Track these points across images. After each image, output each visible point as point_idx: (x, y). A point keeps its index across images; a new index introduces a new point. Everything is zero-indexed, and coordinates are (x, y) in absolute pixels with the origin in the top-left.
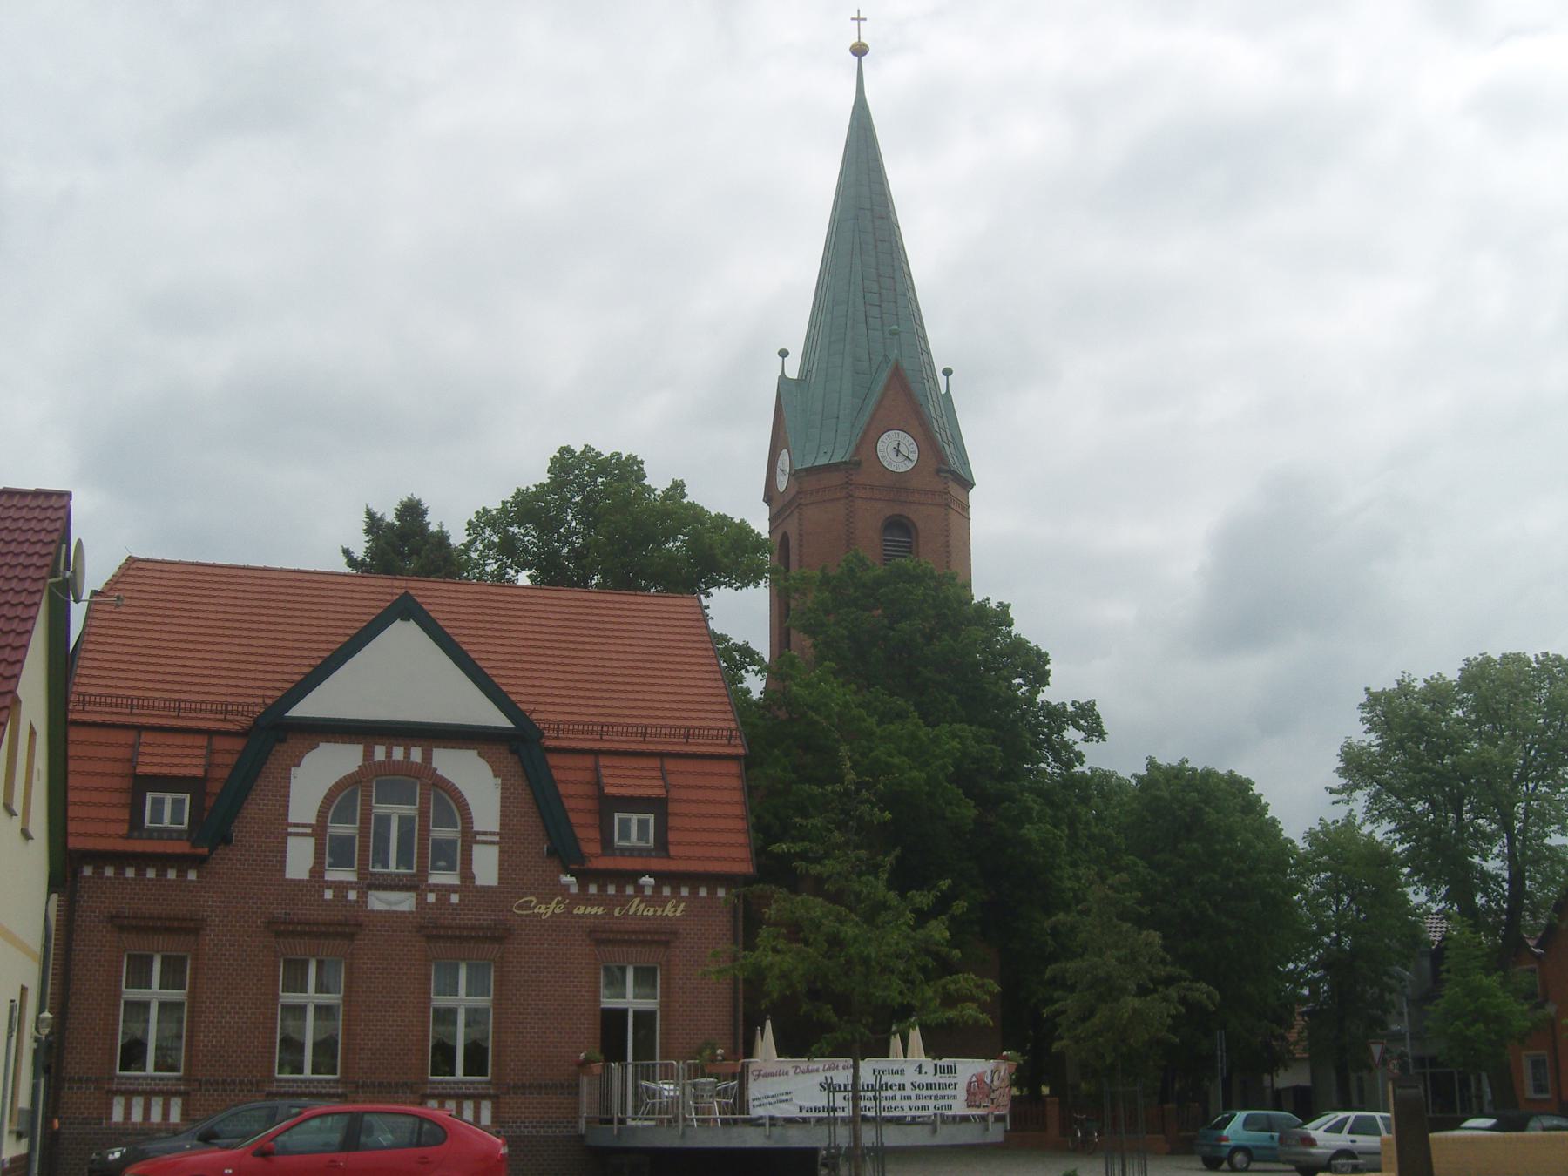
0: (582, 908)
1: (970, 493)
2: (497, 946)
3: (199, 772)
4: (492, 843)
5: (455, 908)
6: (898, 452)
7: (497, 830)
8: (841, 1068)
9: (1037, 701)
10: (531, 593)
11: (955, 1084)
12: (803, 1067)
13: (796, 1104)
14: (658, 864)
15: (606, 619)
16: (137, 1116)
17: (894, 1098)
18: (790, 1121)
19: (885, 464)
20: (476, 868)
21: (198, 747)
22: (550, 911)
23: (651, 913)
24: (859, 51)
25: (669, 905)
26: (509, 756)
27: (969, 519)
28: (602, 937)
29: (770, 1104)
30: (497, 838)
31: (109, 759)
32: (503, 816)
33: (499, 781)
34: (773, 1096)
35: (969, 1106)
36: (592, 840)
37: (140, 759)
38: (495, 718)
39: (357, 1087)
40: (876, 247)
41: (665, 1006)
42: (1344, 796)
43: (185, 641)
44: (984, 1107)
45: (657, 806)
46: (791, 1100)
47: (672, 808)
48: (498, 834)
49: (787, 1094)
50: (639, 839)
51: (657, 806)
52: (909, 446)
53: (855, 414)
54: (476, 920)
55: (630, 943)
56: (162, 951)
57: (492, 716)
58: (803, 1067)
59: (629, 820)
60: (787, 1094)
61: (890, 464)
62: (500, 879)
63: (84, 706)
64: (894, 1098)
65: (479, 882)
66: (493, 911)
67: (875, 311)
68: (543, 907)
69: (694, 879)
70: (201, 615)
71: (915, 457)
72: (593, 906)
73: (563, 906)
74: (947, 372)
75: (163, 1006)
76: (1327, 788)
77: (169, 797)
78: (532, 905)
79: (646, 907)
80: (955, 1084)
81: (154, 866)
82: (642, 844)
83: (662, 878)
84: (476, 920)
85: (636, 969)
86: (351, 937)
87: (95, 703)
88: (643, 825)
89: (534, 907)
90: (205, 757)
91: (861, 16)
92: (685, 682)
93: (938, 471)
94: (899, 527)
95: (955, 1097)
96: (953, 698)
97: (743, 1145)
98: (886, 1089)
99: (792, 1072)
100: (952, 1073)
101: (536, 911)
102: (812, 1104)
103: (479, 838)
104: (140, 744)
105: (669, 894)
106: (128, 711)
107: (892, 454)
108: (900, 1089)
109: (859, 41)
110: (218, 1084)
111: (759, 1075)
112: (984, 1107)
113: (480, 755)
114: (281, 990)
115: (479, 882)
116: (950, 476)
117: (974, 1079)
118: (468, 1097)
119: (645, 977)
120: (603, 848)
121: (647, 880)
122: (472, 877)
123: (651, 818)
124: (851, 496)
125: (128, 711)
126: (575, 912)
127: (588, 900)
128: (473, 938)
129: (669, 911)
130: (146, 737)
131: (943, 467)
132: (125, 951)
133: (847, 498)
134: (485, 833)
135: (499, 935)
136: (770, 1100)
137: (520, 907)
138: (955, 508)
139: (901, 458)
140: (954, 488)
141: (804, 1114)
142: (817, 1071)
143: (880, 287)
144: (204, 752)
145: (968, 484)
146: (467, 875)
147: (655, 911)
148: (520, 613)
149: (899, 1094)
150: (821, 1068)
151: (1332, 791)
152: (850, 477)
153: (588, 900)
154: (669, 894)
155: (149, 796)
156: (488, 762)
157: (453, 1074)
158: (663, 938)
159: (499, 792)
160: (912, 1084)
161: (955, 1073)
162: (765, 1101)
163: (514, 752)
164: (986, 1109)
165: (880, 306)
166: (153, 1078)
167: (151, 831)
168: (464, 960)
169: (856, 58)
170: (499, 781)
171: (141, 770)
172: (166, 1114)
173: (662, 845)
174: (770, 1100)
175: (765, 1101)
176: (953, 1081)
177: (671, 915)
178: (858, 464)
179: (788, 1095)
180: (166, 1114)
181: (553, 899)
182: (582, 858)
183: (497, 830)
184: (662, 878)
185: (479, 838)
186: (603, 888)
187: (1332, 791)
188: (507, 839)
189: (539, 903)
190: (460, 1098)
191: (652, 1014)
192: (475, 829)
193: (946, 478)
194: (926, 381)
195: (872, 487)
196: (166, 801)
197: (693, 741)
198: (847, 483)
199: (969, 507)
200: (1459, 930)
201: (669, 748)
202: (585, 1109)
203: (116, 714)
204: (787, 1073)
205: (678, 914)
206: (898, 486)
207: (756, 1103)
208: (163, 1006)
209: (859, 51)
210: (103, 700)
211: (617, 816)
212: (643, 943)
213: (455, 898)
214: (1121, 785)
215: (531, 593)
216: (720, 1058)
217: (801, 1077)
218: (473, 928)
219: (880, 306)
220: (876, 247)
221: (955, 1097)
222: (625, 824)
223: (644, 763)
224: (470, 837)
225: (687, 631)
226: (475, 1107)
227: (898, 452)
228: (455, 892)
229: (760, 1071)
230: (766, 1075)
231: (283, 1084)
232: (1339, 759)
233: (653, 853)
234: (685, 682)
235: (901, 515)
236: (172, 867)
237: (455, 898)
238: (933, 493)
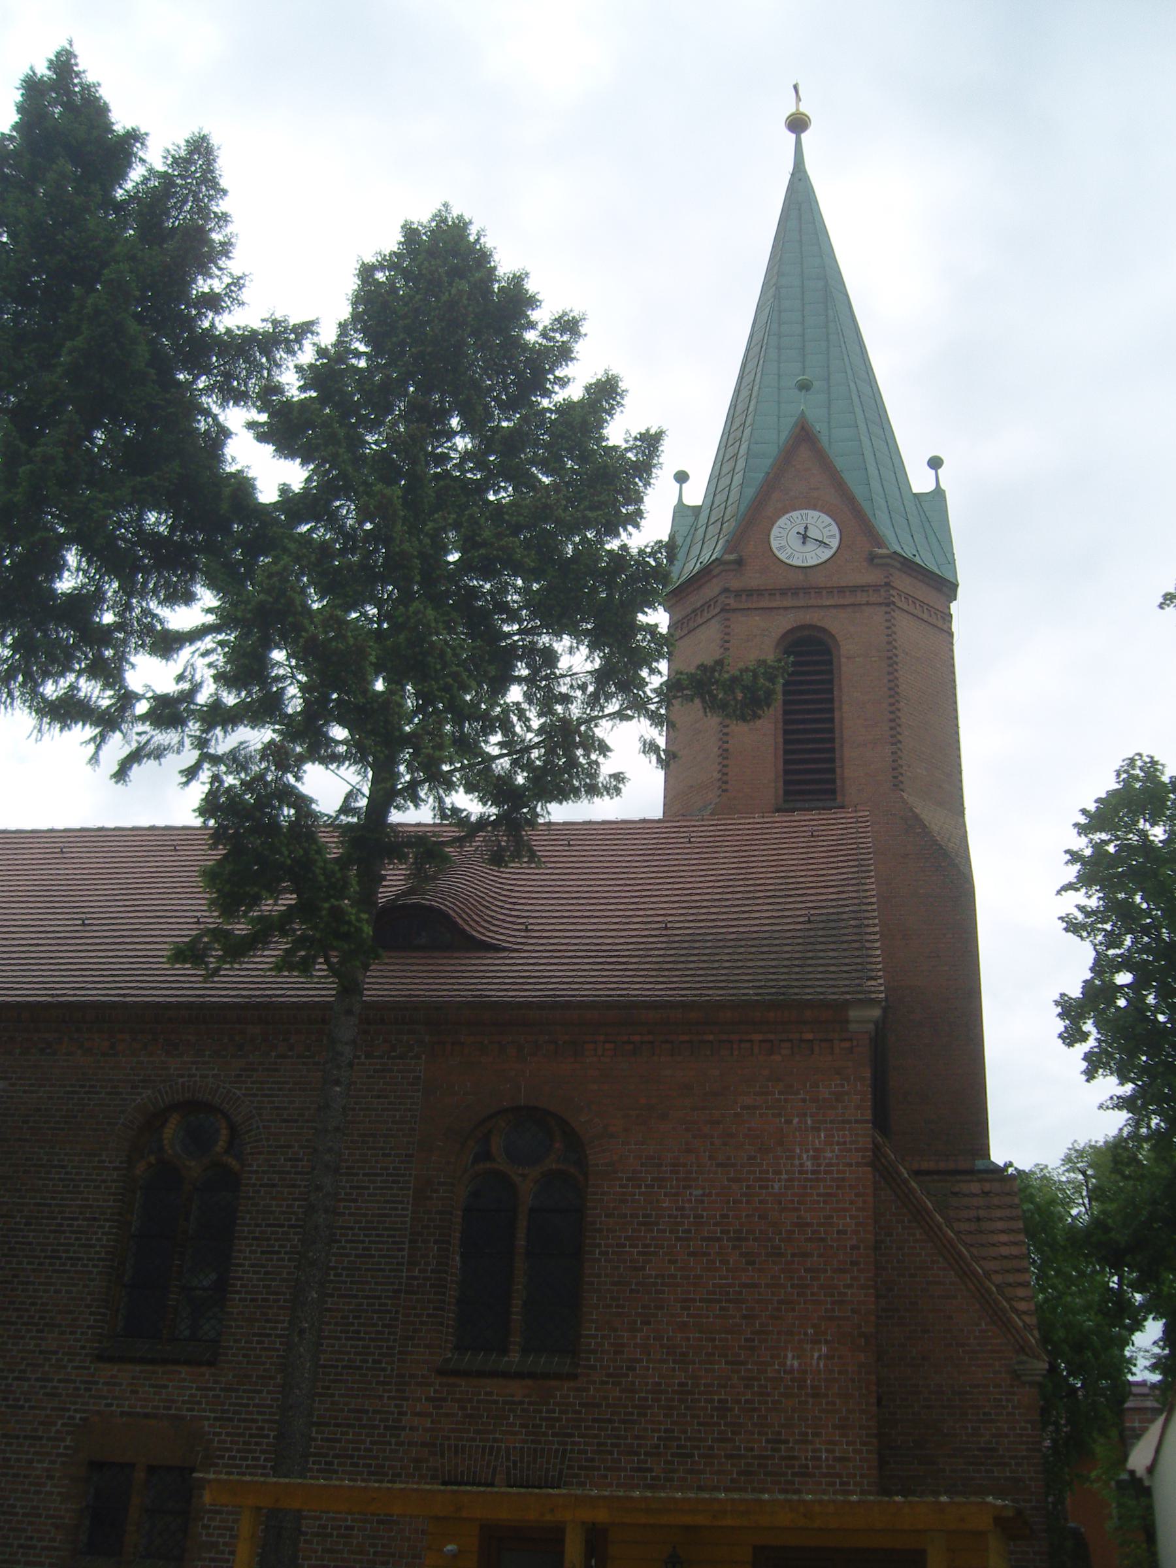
6: (805, 538)
9: (458, 419)
15: (99, 887)
24: (798, 124)
27: (951, 635)
43: (708, 887)
52: (823, 526)
61: (779, 549)
70: (708, 879)
71: (835, 543)
74: (935, 463)
107: (795, 542)
109: (797, 110)
131: (880, 551)
138: (905, 607)
139: (811, 546)
152: (900, 778)
200: (302, 568)
209: (798, 124)
214: (108, 127)
225: (665, 875)
227: (805, 538)
234: (682, 918)
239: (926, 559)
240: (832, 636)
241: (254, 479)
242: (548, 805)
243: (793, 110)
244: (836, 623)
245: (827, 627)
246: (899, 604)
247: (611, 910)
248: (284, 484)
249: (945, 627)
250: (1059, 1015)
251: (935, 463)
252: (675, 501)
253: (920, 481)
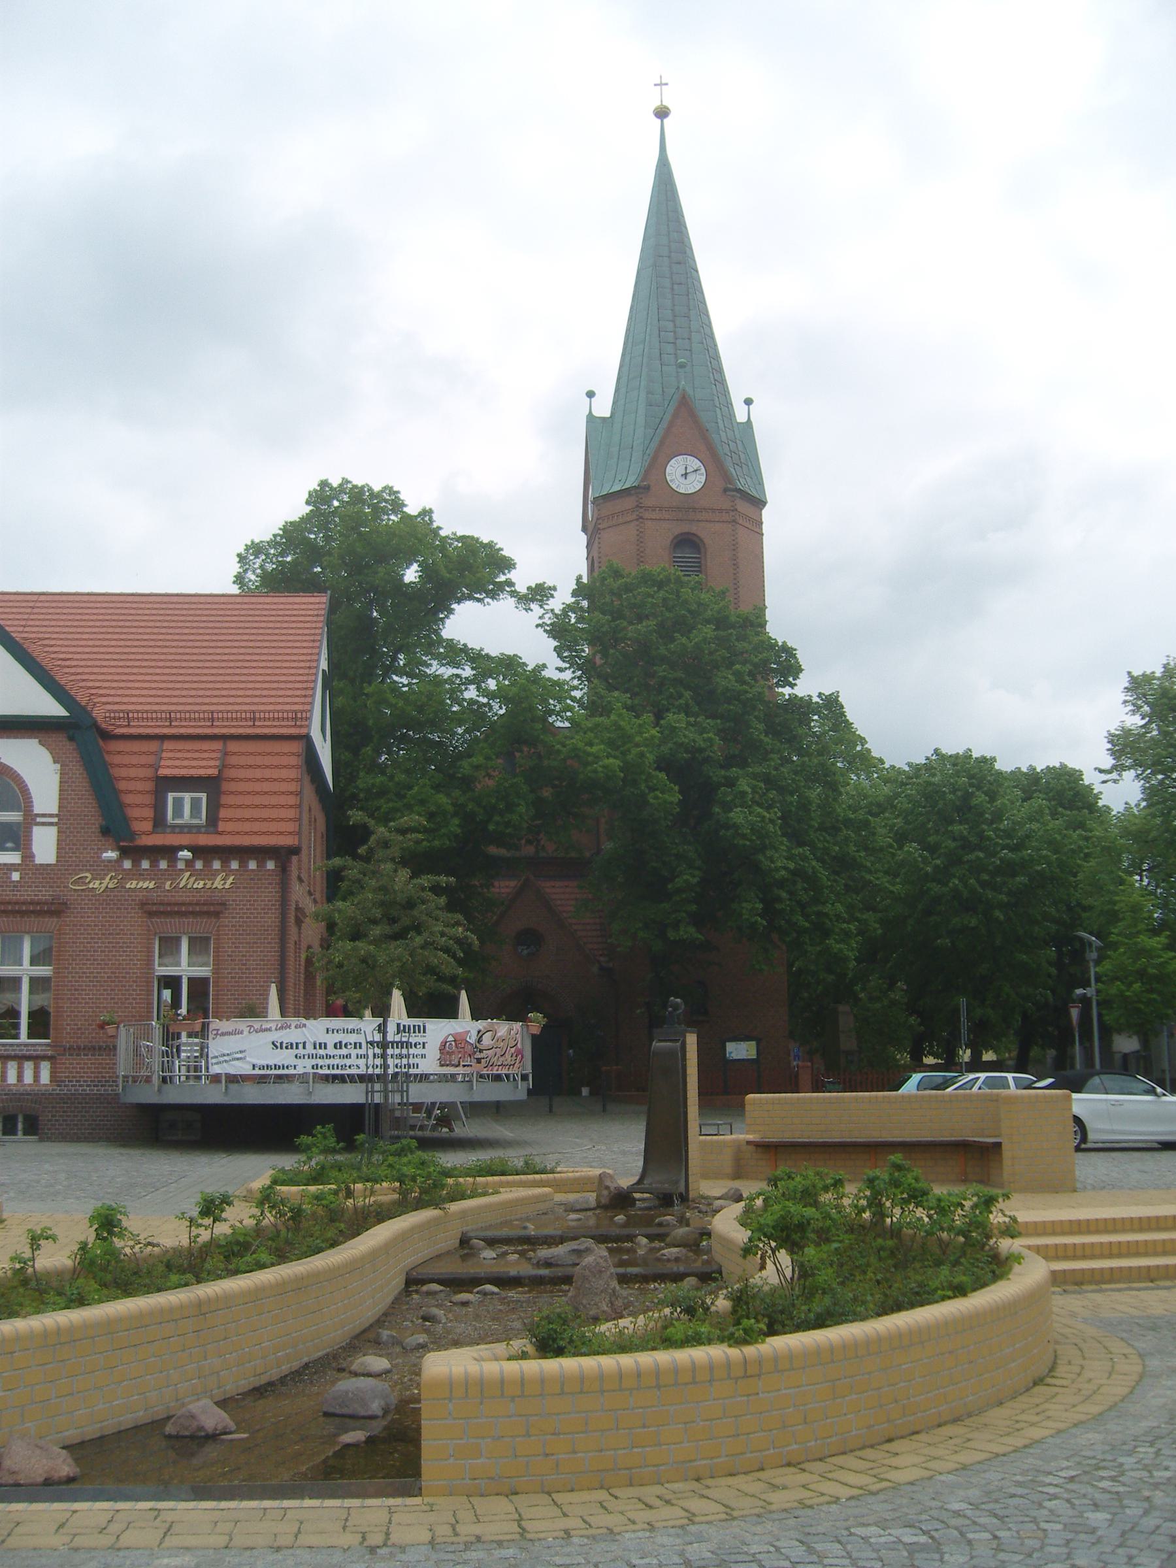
0: (135, 882)
1: (763, 511)
2: (55, 920)
3: (213, 772)
4: (51, 824)
5: (16, 885)
7: (56, 811)
8: (293, 1027)
10: (239, 600)
11: (424, 1043)
12: (257, 1026)
13: (250, 1062)
14: (204, 840)
16: (28, 1078)
17: (348, 1056)
18: (244, 1078)
19: (674, 486)
20: (36, 848)
21: (214, 751)
22: (104, 886)
23: (201, 886)
24: (662, 113)
25: (219, 878)
26: (68, 743)
27: (763, 534)
28: (153, 909)
29: (226, 1061)
30: (55, 820)
31: (143, 766)
32: (61, 799)
33: (58, 766)
34: (228, 1055)
35: (442, 1065)
36: (145, 819)
37: (163, 763)
38: (52, 708)
39: (65, 1050)
40: (672, 289)
41: (216, 971)
42: (1114, 775)
44: (464, 1066)
45: (211, 785)
46: (244, 1058)
47: (225, 786)
48: (57, 815)
49: (241, 1052)
50: (192, 816)
51: (211, 785)
53: (647, 442)
54: (13, 895)
55: (180, 914)
56: (188, 933)
57: (48, 706)
58: (257, 1026)
59: (182, 799)
60: (241, 1052)
61: (671, 481)
62: (57, 857)
63: (171, 722)
64: (348, 1056)
65: (39, 860)
66: (50, 887)
67: (669, 348)
68: (98, 882)
69: (243, 853)
72: (145, 880)
73: (116, 881)
74: (748, 402)
75: (33, 981)
76: (1096, 769)
77: (187, 797)
78: (88, 880)
79: (196, 880)
80: (424, 1043)
81: (255, 859)
82: (195, 821)
83: (198, 851)
84: (35, 895)
85: (191, 940)
86: (217, 914)
87: (147, 718)
88: (195, 804)
89: (89, 882)
90: (219, 759)
91: (663, 82)
92: (252, 671)
93: (726, 490)
94: (688, 543)
95: (424, 1056)
96: (688, 694)
97: (205, 1102)
98: (341, 1048)
99: (246, 1033)
100: (419, 1032)
101: (91, 886)
102: (264, 1063)
103: (38, 820)
104: (162, 751)
105: (219, 867)
106: (210, 724)
108: (355, 1048)
110: (94, 1049)
111: (216, 1035)
112: (464, 1066)
113: (40, 743)
114: (157, 962)
115: (39, 860)
116: (739, 495)
117: (451, 1038)
118: (44, 1058)
119: (199, 945)
120: (155, 826)
121: (186, 854)
122: (32, 856)
123: (204, 796)
124: (641, 518)
125: (210, 724)
126: (128, 886)
127: (140, 874)
128: (32, 912)
129: (218, 883)
130: (168, 745)
132: (155, 934)
133: (637, 520)
134: (44, 815)
135: (56, 909)
136: (226, 1058)
137: (75, 883)
139: (691, 478)
140: (743, 507)
141: (257, 1072)
142: (269, 1030)
143: (675, 326)
144: (218, 755)
145: (760, 503)
146: (28, 856)
147: (205, 884)
148: (190, 618)
149: (354, 1052)
150: (273, 1028)
151: (1101, 771)
153: (140, 874)
154: (219, 867)
155: (171, 796)
156: (48, 749)
157: (17, 1036)
158: (212, 909)
159: (57, 778)
160: (273, 1043)
161: (424, 1032)
162: (222, 1059)
163: (71, 739)
164: (469, 1068)
165: (674, 343)
166: (26, 1045)
167: (174, 827)
168: (28, 933)
169: (659, 121)
170: (58, 766)
171: (163, 772)
172: (20, 1077)
173: (213, 819)
174: (226, 1058)
175: (222, 1059)
176: (421, 1040)
177: (220, 887)
178: (648, 488)
179: (242, 1053)
180: (20, 1077)
181: (107, 875)
182: (133, 835)
183: (56, 811)
184: (198, 851)
185: (38, 820)
186: (154, 863)
187: (1101, 771)
188: (64, 820)
189: (93, 879)
190: (21, 1059)
191: (205, 981)
192: (36, 812)
193: (733, 496)
194: (718, 410)
195: (661, 509)
196: (186, 800)
197: (218, 724)
198: (637, 506)
199: (762, 523)
201: (233, 731)
202: (122, 1068)
203: (226, 726)
204: (242, 1033)
205: (227, 886)
206: (687, 505)
207: (214, 1061)
208: (33, 981)
209: (662, 113)
210: (140, 715)
211: (171, 796)
212: (194, 914)
213: (16, 876)
215: (239, 600)
216: (180, 1018)
217: (254, 1036)
218: (32, 903)
219: (674, 343)
220: (672, 289)
221: (424, 1056)
222: (178, 803)
223: (206, 745)
224: (31, 819)
226: (19, 1068)
228: (16, 870)
229: (218, 1030)
230: (223, 1034)
231: (37, 1048)
232: (1106, 740)
233: (203, 830)
234: (105, 663)
235: (688, 533)
236: (234, 859)
237: (16, 876)
238: (721, 511)
239: (754, 493)
240: (701, 540)
241: (427, 513)
242: (321, 601)
243: (659, 103)
244: (704, 531)
245: (699, 534)
246: (740, 522)
247: (82, 646)
248: (515, 564)
249: (758, 531)
250: (406, 506)
251: (748, 402)
252: (587, 413)
253: (741, 416)
